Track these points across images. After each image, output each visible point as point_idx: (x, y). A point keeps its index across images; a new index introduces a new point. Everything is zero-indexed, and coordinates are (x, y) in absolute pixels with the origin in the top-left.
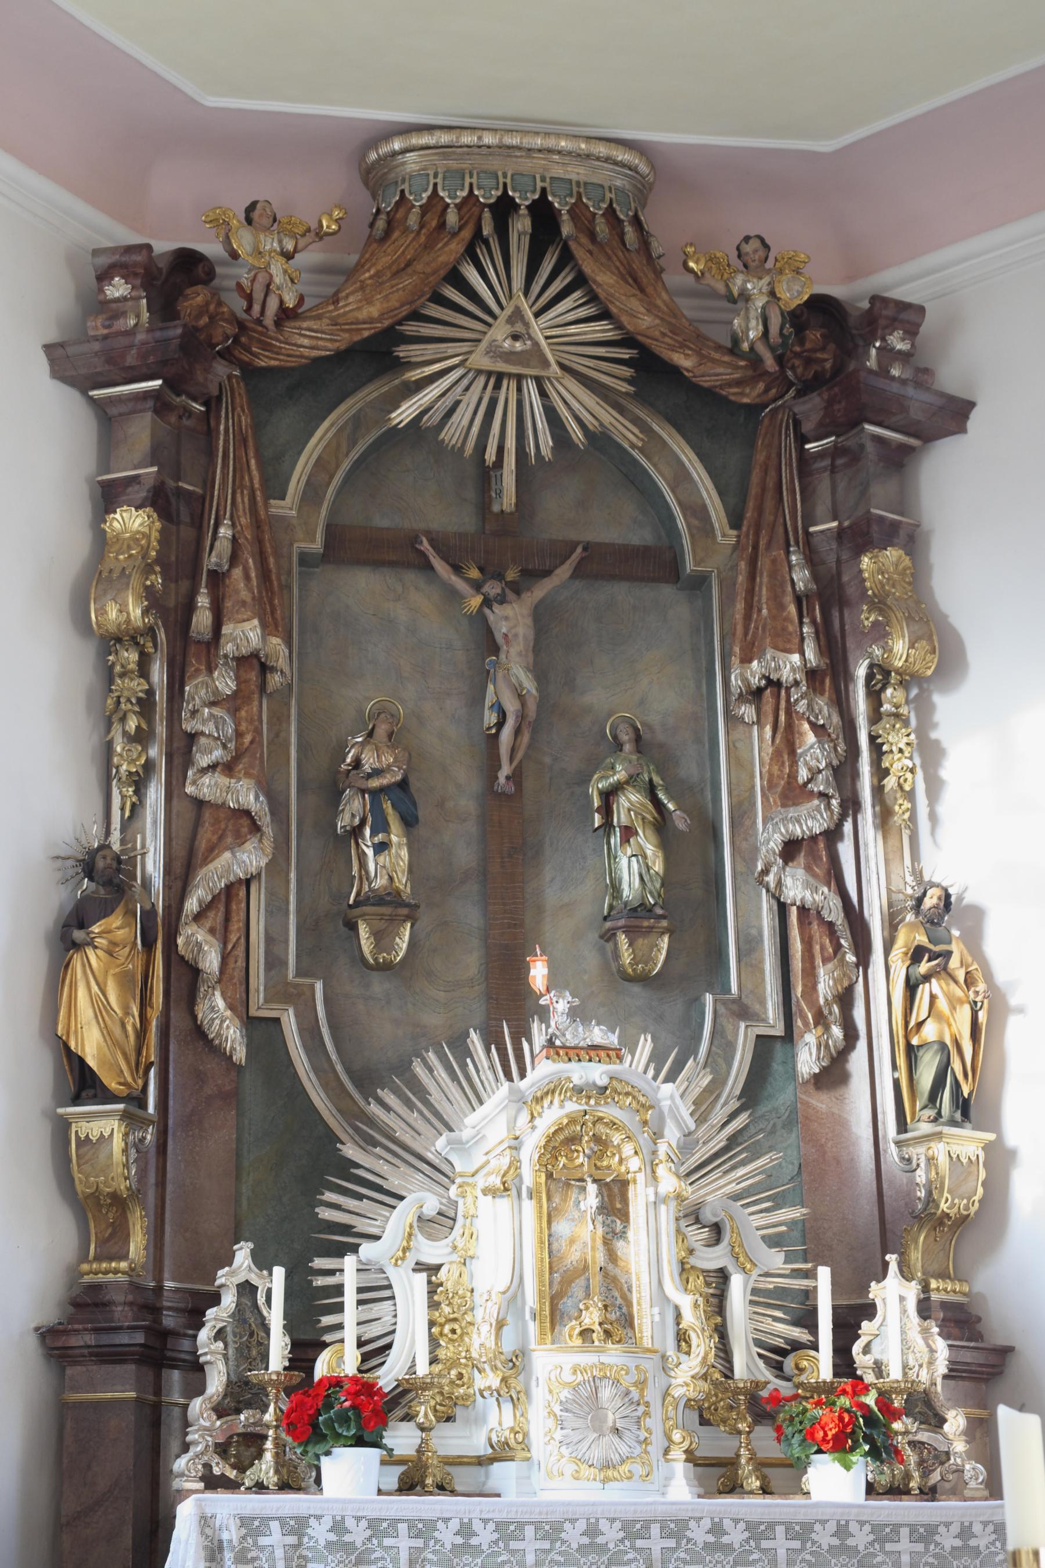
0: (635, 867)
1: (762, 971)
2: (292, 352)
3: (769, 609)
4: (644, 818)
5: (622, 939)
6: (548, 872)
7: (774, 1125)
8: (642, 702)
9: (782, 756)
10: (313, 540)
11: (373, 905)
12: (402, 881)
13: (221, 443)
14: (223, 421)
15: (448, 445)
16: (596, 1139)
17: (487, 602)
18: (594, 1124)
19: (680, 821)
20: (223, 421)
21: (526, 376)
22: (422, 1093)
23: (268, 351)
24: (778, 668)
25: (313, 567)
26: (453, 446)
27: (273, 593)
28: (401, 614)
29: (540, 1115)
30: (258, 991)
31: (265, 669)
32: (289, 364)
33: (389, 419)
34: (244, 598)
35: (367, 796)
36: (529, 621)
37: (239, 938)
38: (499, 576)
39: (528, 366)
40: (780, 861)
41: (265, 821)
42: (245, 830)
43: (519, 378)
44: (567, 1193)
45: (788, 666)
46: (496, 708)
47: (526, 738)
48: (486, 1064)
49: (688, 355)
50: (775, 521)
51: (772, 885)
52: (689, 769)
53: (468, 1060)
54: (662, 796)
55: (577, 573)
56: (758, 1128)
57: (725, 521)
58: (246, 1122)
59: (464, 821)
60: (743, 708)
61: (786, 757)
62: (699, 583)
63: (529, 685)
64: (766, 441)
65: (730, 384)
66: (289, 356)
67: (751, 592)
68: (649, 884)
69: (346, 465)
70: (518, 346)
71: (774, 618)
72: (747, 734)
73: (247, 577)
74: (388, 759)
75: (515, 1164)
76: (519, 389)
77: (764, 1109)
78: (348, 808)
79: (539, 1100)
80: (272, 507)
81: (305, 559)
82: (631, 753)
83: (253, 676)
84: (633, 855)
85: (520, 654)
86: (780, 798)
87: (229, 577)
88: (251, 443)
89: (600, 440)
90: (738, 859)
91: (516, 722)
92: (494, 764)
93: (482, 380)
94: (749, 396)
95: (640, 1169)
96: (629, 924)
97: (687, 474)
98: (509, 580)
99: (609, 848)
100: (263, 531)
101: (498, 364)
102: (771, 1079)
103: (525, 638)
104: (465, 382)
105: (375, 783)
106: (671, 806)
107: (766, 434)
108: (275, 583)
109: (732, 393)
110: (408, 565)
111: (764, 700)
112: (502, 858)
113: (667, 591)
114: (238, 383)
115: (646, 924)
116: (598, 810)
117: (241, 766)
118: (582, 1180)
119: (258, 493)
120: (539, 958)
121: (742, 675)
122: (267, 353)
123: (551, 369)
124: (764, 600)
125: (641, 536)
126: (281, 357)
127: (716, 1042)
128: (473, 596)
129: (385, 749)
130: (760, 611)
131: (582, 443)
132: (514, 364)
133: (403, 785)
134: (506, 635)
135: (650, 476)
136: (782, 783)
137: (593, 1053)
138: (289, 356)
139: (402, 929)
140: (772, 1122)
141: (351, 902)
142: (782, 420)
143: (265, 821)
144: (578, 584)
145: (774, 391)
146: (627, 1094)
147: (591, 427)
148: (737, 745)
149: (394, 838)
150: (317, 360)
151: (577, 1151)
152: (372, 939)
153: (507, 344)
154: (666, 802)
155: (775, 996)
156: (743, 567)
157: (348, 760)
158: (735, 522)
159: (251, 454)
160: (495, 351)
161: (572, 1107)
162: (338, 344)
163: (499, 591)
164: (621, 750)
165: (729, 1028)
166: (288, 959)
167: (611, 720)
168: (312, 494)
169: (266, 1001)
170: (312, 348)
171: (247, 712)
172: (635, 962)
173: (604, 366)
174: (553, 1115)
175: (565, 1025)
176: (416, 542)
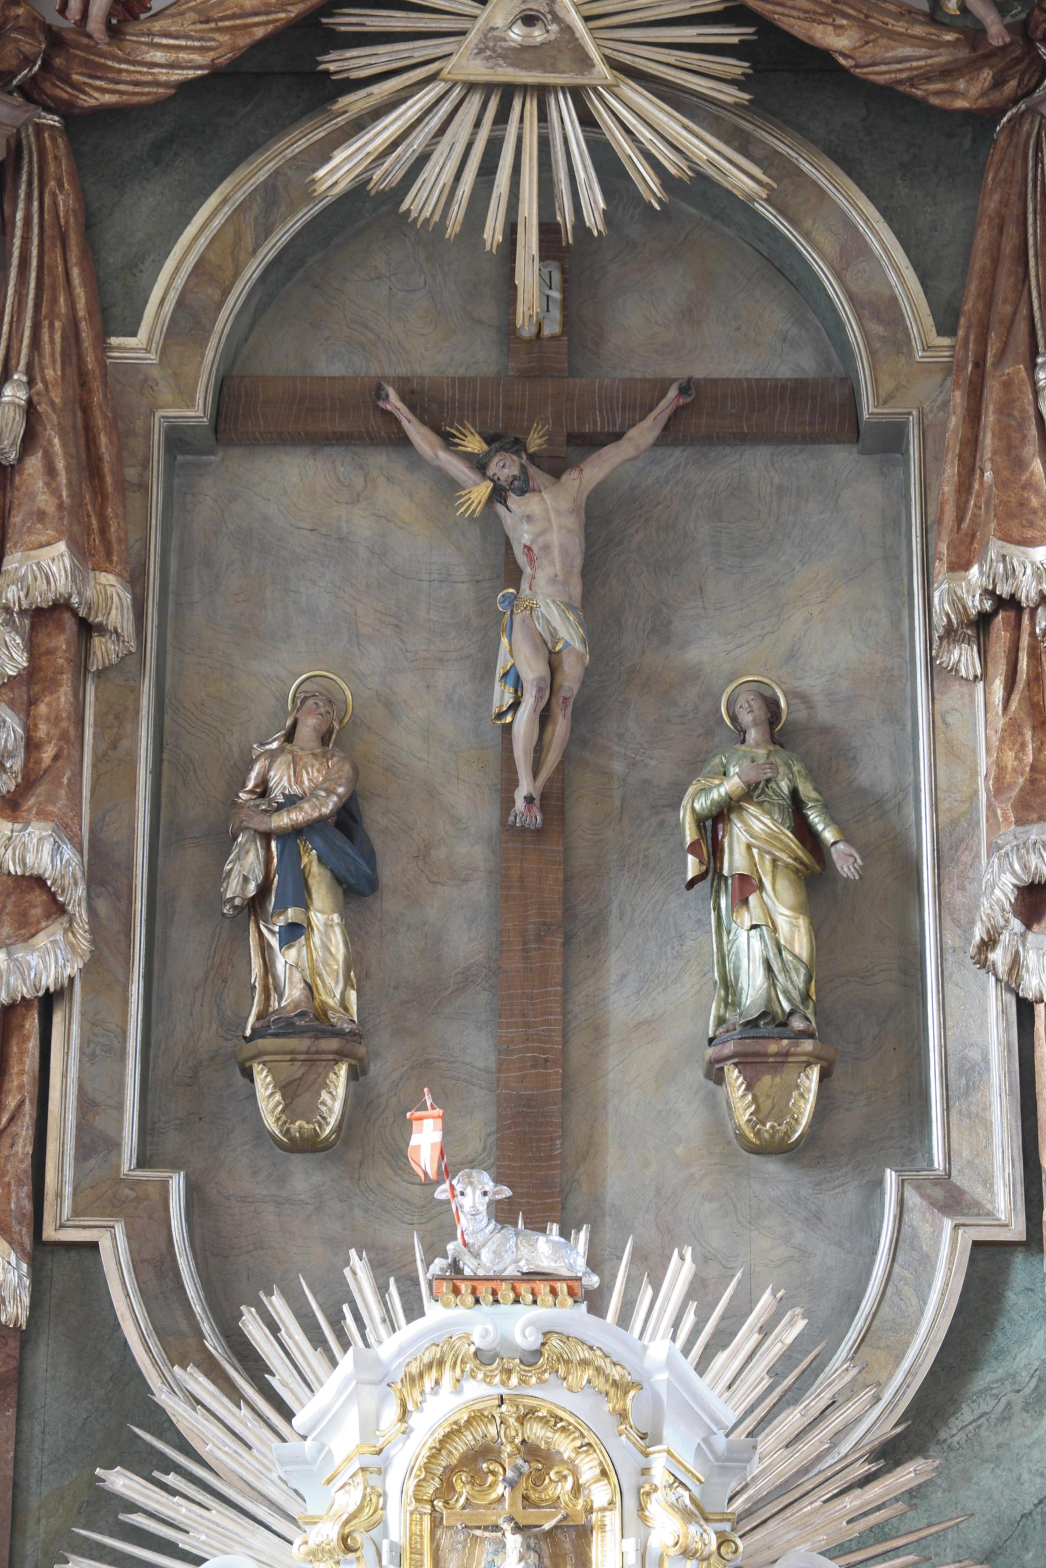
0: (763, 943)
1: (987, 1126)
2: (139, 77)
3: (996, 472)
4: (775, 861)
5: (733, 1074)
6: (615, 964)
7: (1009, 1404)
8: (792, 655)
9: (1021, 734)
10: (191, 404)
11: (276, 1035)
12: (334, 991)
13: (17, 242)
14: (21, 205)
15: (417, 219)
16: (530, 1451)
17: (499, 494)
18: (521, 1420)
19: (845, 860)
20: (21, 205)
21: (553, 89)
22: (255, 1367)
23: (100, 78)
24: (1010, 574)
25: (200, 452)
26: (427, 221)
27: (104, 497)
28: (361, 525)
29: (419, 1406)
30: (59, 1195)
31: (87, 629)
32: (136, 99)
33: (313, 182)
34: (43, 506)
35: (273, 844)
36: (572, 522)
37: (21, 1104)
38: (517, 446)
39: (554, 70)
40: (1017, 925)
41: (76, 896)
42: (37, 912)
43: (542, 92)
44: (472, 1554)
45: (1029, 571)
46: (511, 678)
47: (561, 727)
48: (377, 1312)
49: (841, 27)
50: (1015, 314)
51: (1002, 969)
52: (874, 771)
53: (346, 1308)
54: (815, 818)
55: (671, 434)
56: (977, 1413)
57: (929, 321)
58: (37, 1429)
59: (466, 880)
60: (956, 653)
61: (1028, 734)
62: (890, 440)
63: (569, 633)
64: (1001, 175)
65: (927, 76)
66: (136, 84)
67: (972, 443)
68: (781, 978)
69: (252, 270)
70: (538, 35)
71: (1002, 484)
72: (967, 700)
73: (51, 471)
74: (312, 775)
75: (373, 1502)
76: (543, 117)
77: (990, 1377)
78: (237, 867)
79: (414, 1380)
80: (112, 348)
81: (178, 440)
82: (758, 745)
83: (61, 641)
84: (754, 927)
85: (554, 580)
86: (1015, 808)
87: (21, 472)
88: (73, 240)
89: (697, 190)
90: (948, 922)
91: (538, 698)
92: (511, 782)
93: (474, 102)
94: (968, 93)
95: (611, 1503)
96: (740, 1049)
97: (861, 243)
98: (531, 450)
99: (719, 918)
100: (90, 392)
101: (499, 70)
102: (1003, 1321)
103: (565, 552)
104: (446, 107)
105: (284, 820)
106: (829, 836)
107: (1002, 160)
108: (109, 479)
109: (930, 91)
110: (370, 440)
111: (993, 635)
112: (525, 943)
113: (842, 458)
114: (53, 139)
115: (773, 1047)
116: (694, 849)
117: (32, 800)
118: (496, 1528)
119: (83, 325)
120: (430, 1112)
121: (951, 592)
122: (98, 83)
123: (595, 70)
124: (988, 454)
125: (796, 363)
126: (122, 87)
127: (900, 1258)
128: (476, 484)
129: (310, 760)
130: (982, 472)
131: (659, 201)
132: (529, 68)
133: (347, 820)
134: (528, 549)
135: (800, 253)
136: (1021, 781)
137: (524, 1288)
138: (136, 84)
139: (332, 1076)
140: (1004, 1401)
141: (248, 1032)
142: (1029, 135)
143: (76, 896)
144: (678, 455)
145: (1013, 83)
146: (584, 1363)
147: (673, 171)
148: (949, 719)
149: (317, 919)
150: (185, 87)
151: (493, 1473)
152: (278, 1097)
153: (517, 34)
154: (820, 827)
155: (1009, 1169)
156: (958, 400)
157: (250, 785)
158: (946, 326)
159: (74, 256)
160: (492, 48)
161: (477, 1390)
162: (212, 54)
163: (515, 471)
164: (743, 742)
165: (925, 1230)
166: (121, 1137)
167: (729, 690)
168: (188, 322)
169: (76, 1213)
170: (172, 66)
171: (48, 704)
172: (759, 1117)
173: (693, 59)
174: (442, 1405)
175: (481, 1238)
176: (378, 397)
